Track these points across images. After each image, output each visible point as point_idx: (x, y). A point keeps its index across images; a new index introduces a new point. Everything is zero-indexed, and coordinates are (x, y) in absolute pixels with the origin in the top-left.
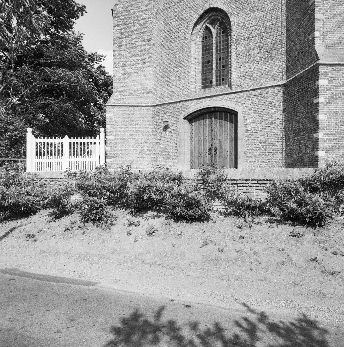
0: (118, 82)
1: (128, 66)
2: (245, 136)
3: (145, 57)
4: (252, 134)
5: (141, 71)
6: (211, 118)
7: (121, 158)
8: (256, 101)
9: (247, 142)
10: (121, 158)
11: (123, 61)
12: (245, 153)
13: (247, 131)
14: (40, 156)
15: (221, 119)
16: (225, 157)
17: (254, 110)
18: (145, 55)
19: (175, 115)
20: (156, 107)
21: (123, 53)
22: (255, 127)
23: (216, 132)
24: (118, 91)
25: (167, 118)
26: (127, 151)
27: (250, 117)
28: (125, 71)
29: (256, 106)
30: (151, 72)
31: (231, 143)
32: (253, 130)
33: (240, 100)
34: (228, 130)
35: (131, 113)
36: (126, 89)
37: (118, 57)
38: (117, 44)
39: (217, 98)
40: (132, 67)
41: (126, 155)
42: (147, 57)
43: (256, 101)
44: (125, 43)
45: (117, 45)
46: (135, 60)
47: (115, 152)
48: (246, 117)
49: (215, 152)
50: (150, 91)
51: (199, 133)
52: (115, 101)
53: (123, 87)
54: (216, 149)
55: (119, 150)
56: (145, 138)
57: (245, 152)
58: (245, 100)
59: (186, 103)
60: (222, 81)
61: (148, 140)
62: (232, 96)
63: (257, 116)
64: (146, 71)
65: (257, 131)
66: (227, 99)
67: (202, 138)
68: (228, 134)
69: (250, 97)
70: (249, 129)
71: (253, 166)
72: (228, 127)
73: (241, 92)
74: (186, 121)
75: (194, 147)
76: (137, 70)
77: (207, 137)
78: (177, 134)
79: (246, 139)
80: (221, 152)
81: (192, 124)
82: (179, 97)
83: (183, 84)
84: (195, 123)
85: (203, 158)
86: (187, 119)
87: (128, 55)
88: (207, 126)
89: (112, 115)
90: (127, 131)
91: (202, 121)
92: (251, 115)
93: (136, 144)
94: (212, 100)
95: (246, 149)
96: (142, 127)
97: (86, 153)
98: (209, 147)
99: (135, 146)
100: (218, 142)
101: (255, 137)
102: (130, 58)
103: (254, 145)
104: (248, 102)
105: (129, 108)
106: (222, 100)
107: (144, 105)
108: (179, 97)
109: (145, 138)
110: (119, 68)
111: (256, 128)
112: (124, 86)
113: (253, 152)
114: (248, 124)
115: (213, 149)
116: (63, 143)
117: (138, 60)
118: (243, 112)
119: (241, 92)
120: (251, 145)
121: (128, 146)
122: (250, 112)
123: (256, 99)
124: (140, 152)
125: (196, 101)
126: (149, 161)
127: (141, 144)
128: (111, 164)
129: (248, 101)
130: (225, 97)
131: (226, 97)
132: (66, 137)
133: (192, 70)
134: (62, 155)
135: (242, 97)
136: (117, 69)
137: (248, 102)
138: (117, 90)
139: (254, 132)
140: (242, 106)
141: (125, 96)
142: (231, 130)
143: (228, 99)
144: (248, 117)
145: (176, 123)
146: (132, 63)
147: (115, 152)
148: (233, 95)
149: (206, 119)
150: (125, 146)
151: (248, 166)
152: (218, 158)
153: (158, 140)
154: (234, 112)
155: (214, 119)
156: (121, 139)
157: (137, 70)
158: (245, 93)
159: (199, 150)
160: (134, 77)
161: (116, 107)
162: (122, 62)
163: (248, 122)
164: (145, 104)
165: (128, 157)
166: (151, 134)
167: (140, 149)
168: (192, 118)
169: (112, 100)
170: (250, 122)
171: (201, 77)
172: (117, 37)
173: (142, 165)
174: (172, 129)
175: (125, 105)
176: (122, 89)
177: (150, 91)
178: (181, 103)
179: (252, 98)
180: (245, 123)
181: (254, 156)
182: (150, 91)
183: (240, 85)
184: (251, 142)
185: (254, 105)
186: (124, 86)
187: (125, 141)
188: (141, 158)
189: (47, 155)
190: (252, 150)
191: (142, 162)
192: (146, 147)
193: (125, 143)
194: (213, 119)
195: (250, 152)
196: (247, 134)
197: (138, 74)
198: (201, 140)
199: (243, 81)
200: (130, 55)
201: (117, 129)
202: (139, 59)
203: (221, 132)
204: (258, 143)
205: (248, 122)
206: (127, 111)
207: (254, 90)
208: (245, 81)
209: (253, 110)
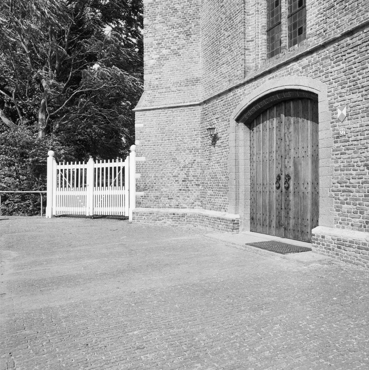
0: (151, 73)
1: (165, 45)
2: (333, 151)
3: (189, 26)
4: (347, 144)
5: (184, 49)
6: (279, 116)
7: (156, 190)
8: (357, 60)
9: (337, 165)
10: (156, 190)
11: (157, 40)
12: (333, 191)
13: (338, 137)
14: (119, 187)
15: (297, 115)
16: (304, 197)
17: (351, 84)
18: (188, 22)
19: (224, 115)
20: (205, 106)
21: (158, 27)
22: (355, 126)
23: (288, 143)
24: (152, 87)
25: (216, 122)
26: (164, 179)
27: (342, 103)
28: (161, 54)
29: (356, 74)
30: (200, 49)
31: (314, 164)
32: (349, 135)
33: (324, 67)
34: (309, 138)
35: (169, 119)
36: (162, 82)
37: (151, 35)
38: (148, 14)
39: (282, 72)
40: (171, 46)
41: (162, 186)
42: (193, 25)
43: (357, 60)
44: (160, 10)
45: (149, 16)
46: (176, 35)
47: (148, 181)
48: (335, 105)
49: (286, 185)
50: (198, 80)
51: (263, 146)
52: (147, 103)
53: (159, 80)
54: (288, 177)
55: (153, 178)
56: (191, 158)
57: (334, 188)
58: (333, 64)
59: (239, 91)
60: (298, 36)
61: (195, 160)
62: (307, 61)
63: (360, 99)
64: (191, 48)
65: (359, 137)
66: (298, 70)
67: (267, 156)
68: (309, 146)
69: (343, 54)
70: (342, 133)
71: (350, 223)
72: (309, 130)
73: (324, 46)
74: (242, 125)
75: (256, 172)
76: (178, 49)
77: (275, 153)
78: (228, 150)
79: (334, 157)
80: (297, 185)
81: (253, 130)
82: (230, 83)
83: (235, 58)
84: (257, 127)
85: (269, 195)
86: (242, 122)
87: (164, 28)
88: (275, 132)
89: (142, 125)
90: (163, 149)
91: (267, 123)
92: (347, 97)
93: (177, 169)
94: (273, 77)
95: (335, 181)
96: (185, 141)
97: (113, 184)
98: (277, 174)
99: (176, 171)
100: (291, 164)
101: (355, 152)
102: (167, 33)
103: (352, 172)
104: (338, 68)
105: (166, 112)
106: (290, 74)
107: (188, 104)
108: (230, 83)
109: (191, 157)
110: (152, 51)
111: (357, 129)
112: (160, 78)
113: (351, 189)
114: (339, 121)
115: (283, 177)
116: (124, 167)
117: (179, 33)
118: (330, 94)
119: (324, 46)
120: (345, 172)
121: (165, 172)
122: (343, 91)
123: (357, 56)
124: (183, 181)
125: (250, 85)
126: (196, 196)
127: (184, 167)
128: (142, 199)
129: (339, 65)
130: (295, 67)
131: (295, 65)
132: (91, 160)
133: (250, 28)
134: (85, 186)
135: (326, 58)
136: (149, 53)
137: (338, 68)
138: (149, 86)
139: (353, 138)
140: (327, 79)
141: (161, 93)
142: (314, 137)
143: (301, 68)
144: (339, 104)
145: (226, 130)
146: (171, 39)
147: (148, 181)
148: (309, 57)
149: (273, 117)
150: (162, 172)
151: (340, 223)
152: (291, 197)
153: (207, 161)
154: (312, 95)
155: (285, 116)
156: (154, 161)
157: (178, 49)
158: (331, 48)
159: (263, 179)
160: (173, 62)
161: (147, 112)
162: (156, 42)
163: (338, 115)
164: (190, 102)
165: (165, 190)
166: (200, 150)
167: (182, 176)
168: (252, 116)
169: (142, 103)
170: (342, 114)
171: (265, 37)
172: (149, 4)
173: (186, 202)
174: (222, 141)
175: (159, 107)
176: (157, 82)
177: (198, 80)
178: (231, 94)
179: (347, 56)
180: (333, 118)
181: (353, 199)
182: (197, 80)
183: (322, 30)
184: (346, 164)
185: (351, 71)
186: (160, 78)
187: (161, 163)
188: (184, 190)
189: (69, 187)
190: (348, 184)
191: (186, 198)
192: (191, 173)
193: (161, 167)
194: (283, 116)
195: (345, 188)
196: (336, 145)
197: (179, 55)
198: (265, 161)
199: (328, 20)
200: (167, 28)
201: (150, 146)
202: (181, 32)
203: (297, 142)
204: (362, 168)
205: (338, 115)
206: (164, 117)
207: (350, 33)
208: (332, 19)
209: (349, 84)
